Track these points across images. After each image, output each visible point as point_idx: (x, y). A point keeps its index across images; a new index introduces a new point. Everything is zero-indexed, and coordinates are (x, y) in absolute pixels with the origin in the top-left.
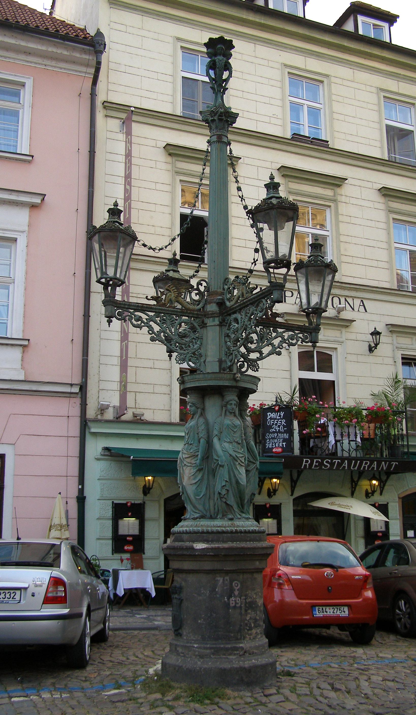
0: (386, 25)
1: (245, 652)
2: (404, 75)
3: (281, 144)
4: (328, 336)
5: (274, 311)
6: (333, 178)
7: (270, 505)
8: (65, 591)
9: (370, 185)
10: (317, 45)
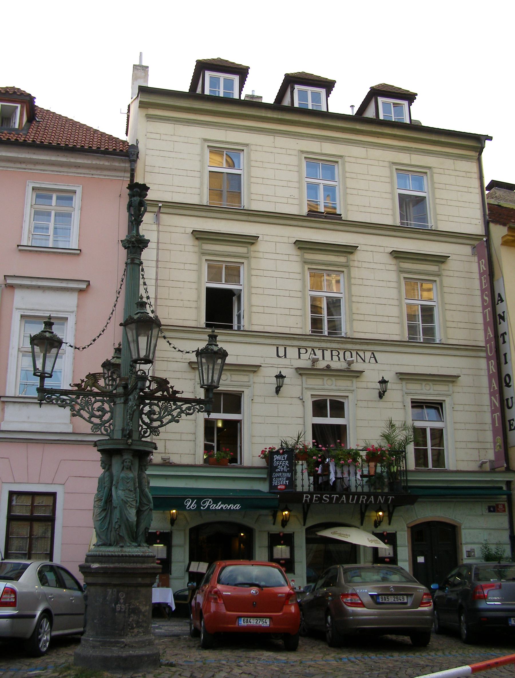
0: (406, 103)
1: (126, 645)
2: (415, 148)
3: (297, 221)
4: (340, 386)
5: (174, 389)
6: (345, 247)
7: (387, 533)
8: (15, 598)
9: (381, 249)
10: (332, 131)
